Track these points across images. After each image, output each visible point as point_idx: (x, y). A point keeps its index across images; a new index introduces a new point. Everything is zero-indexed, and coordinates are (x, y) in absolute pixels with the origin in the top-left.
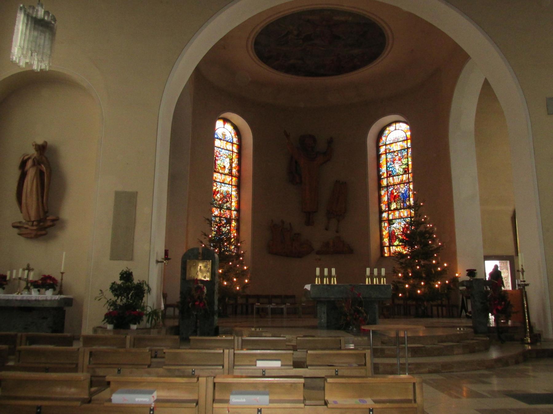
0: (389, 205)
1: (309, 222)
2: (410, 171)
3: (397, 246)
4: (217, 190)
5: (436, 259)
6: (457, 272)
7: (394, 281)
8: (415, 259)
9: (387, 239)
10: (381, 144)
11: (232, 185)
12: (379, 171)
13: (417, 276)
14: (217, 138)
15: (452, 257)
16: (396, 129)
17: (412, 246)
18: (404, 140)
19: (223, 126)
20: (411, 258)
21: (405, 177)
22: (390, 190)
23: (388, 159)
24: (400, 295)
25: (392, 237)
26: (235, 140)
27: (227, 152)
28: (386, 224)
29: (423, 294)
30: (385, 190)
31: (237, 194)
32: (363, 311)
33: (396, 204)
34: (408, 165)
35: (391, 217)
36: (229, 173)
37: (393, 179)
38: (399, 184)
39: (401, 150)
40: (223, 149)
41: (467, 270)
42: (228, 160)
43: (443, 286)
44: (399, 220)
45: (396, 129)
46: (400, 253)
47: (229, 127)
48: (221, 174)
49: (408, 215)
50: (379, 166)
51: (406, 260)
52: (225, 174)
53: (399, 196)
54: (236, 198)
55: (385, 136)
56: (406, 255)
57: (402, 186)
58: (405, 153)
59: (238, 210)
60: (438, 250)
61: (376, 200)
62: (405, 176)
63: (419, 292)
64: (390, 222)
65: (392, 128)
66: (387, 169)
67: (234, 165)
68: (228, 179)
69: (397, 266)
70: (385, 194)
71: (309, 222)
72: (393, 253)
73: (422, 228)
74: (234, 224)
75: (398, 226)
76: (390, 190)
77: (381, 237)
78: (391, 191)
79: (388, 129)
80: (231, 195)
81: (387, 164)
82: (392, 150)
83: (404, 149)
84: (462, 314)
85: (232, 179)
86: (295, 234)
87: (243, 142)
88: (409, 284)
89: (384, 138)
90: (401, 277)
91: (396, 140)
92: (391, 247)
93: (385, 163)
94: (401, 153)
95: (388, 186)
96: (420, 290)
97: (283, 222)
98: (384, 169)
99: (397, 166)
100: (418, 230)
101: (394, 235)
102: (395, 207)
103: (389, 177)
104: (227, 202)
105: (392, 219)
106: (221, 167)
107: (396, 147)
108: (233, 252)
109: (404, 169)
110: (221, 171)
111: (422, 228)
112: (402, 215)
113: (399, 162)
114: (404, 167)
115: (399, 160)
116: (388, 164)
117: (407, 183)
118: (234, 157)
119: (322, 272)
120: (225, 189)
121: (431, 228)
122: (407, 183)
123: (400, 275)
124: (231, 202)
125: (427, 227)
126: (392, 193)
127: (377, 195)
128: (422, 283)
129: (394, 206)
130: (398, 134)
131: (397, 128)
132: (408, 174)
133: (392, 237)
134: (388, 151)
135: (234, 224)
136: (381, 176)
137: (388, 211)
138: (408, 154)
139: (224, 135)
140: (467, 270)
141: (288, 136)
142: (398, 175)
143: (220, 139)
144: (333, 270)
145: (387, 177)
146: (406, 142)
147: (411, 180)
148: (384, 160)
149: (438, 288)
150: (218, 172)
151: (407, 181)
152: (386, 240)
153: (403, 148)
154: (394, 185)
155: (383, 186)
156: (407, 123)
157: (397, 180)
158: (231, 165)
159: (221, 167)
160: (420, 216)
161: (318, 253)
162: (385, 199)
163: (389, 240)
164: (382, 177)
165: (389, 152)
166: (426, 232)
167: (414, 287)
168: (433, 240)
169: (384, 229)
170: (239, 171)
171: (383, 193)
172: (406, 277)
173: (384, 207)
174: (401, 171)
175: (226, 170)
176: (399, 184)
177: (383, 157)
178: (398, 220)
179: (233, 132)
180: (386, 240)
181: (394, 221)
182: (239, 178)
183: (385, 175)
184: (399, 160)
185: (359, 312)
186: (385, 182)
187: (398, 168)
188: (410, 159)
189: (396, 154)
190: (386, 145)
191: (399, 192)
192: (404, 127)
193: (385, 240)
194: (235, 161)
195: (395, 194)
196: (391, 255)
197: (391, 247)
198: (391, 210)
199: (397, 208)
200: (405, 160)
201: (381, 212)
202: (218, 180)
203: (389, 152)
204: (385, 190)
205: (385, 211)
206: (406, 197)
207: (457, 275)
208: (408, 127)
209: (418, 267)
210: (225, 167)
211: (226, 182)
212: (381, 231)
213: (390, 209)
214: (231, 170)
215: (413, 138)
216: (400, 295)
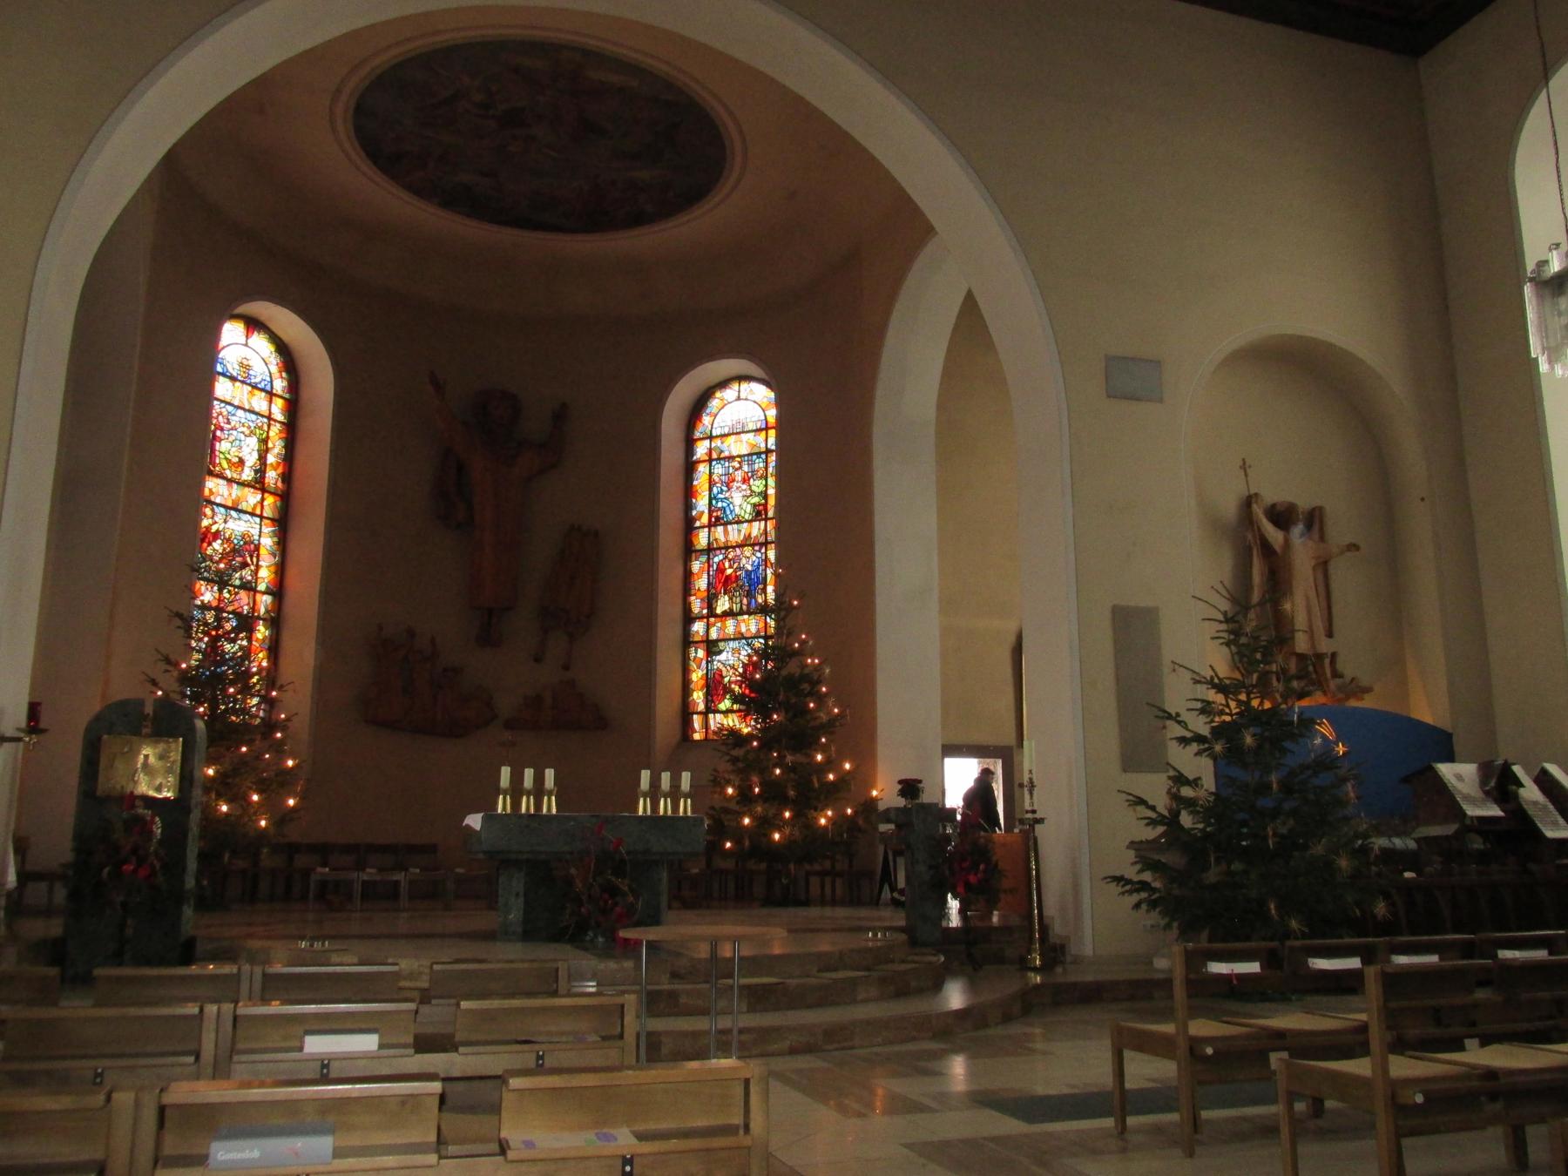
0: (710, 601)
1: (488, 634)
2: (771, 514)
3: (727, 712)
4: (214, 529)
5: (824, 749)
6: (873, 786)
7: (713, 808)
8: (771, 750)
9: (701, 694)
11: (261, 517)
12: (689, 507)
13: (775, 795)
16: (739, 398)
19: (243, 340)
21: (756, 529)
22: (716, 560)
23: (715, 477)
25: (715, 687)
26: (280, 385)
27: (254, 417)
28: (701, 653)
29: (788, 843)
30: (704, 559)
31: (278, 543)
34: (765, 496)
35: (714, 635)
36: (256, 480)
37: (726, 533)
38: (741, 546)
39: (751, 455)
40: (238, 407)
41: (900, 782)
42: (253, 443)
44: (734, 643)
45: (739, 398)
46: (733, 733)
48: (230, 481)
50: (689, 493)
57: (748, 551)
59: (278, 591)
60: (833, 720)
62: (756, 524)
63: (777, 836)
64: (712, 648)
65: (729, 394)
66: (710, 503)
67: (271, 459)
68: (251, 498)
69: (724, 766)
73: (792, 668)
74: (262, 632)
75: (732, 659)
76: (716, 560)
79: (718, 394)
80: (257, 548)
81: (710, 490)
82: (726, 454)
83: (759, 454)
85: (263, 499)
87: (305, 394)
89: (706, 420)
90: (732, 797)
94: (751, 463)
95: (710, 550)
96: (780, 831)
97: (411, 633)
98: (702, 503)
99: (737, 498)
100: (784, 673)
102: (727, 606)
104: (244, 565)
106: (229, 461)
108: (210, 544)
109: (755, 505)
110: (228, 474)
112: (743, 630)
114: (756, 500)
115: (745, 481)
117: (761, 545)
118: (272, 434)
119: (517, 778)
120: (238, 526)
121: (817, 668)
122: (761, 545)
123: (730, 791)
124: (258, 567)
126: (721, 570)
128: (787, 814)
129: (723, 604)
130: (743, 412)
131: (743, 395)
132: (766, 519)
133: (715, 687)
134: (715, 456)
135: (262, 632)
136: (693, 520)
137: (708, 617)
139: (246, 367)
140: (900, 782)
142: (739, 522)
143: (233, 379)
144: (550, 774)
145: (710, 525)
149: (825, 827)
150: (221, 476)
151: (762, 540)
152: (698, 697)
154: (727, 548)
157: (735, 534)
158: (262, 458)
159: (229, 461)
161: (509, 725)
162: (702, 583)
164: (698, 524)
165: (719, 459)
166: (805, 678)
168: (820, 699)
169: (693, 665)
170: (287, 477)
171: (696, 566)
172: (745, 797)
173: (697, 606)
174: (746, 511)
176: (741, 546)
177: (703, 469)
179: (274, 361)
180: (698, 697)
181: (721, 644)
182: (285, 497)
183: (705, 519)
184: (745, 481)
185: (613, 891)
186: (702, 539)
187: (740, 502)
188: (771, 482)
190: (711, 438)
193: (695, 695)
194: (277, 447)
195: (729, 571)
196: (711, 736)
198: (716, 616)
199: (731, 609)
200: (758, 483)
201: (689, 619)
202: (218, 500)
204: (704, 559)
205: (701, 618)
206: (754, 583)
207: (874, 793)
210: (241, 462)
211: (243, 506)
212: (686, 671)
213: (712, 613)
214: (261, 471)
215: (782, 425)
216: (728, 845)
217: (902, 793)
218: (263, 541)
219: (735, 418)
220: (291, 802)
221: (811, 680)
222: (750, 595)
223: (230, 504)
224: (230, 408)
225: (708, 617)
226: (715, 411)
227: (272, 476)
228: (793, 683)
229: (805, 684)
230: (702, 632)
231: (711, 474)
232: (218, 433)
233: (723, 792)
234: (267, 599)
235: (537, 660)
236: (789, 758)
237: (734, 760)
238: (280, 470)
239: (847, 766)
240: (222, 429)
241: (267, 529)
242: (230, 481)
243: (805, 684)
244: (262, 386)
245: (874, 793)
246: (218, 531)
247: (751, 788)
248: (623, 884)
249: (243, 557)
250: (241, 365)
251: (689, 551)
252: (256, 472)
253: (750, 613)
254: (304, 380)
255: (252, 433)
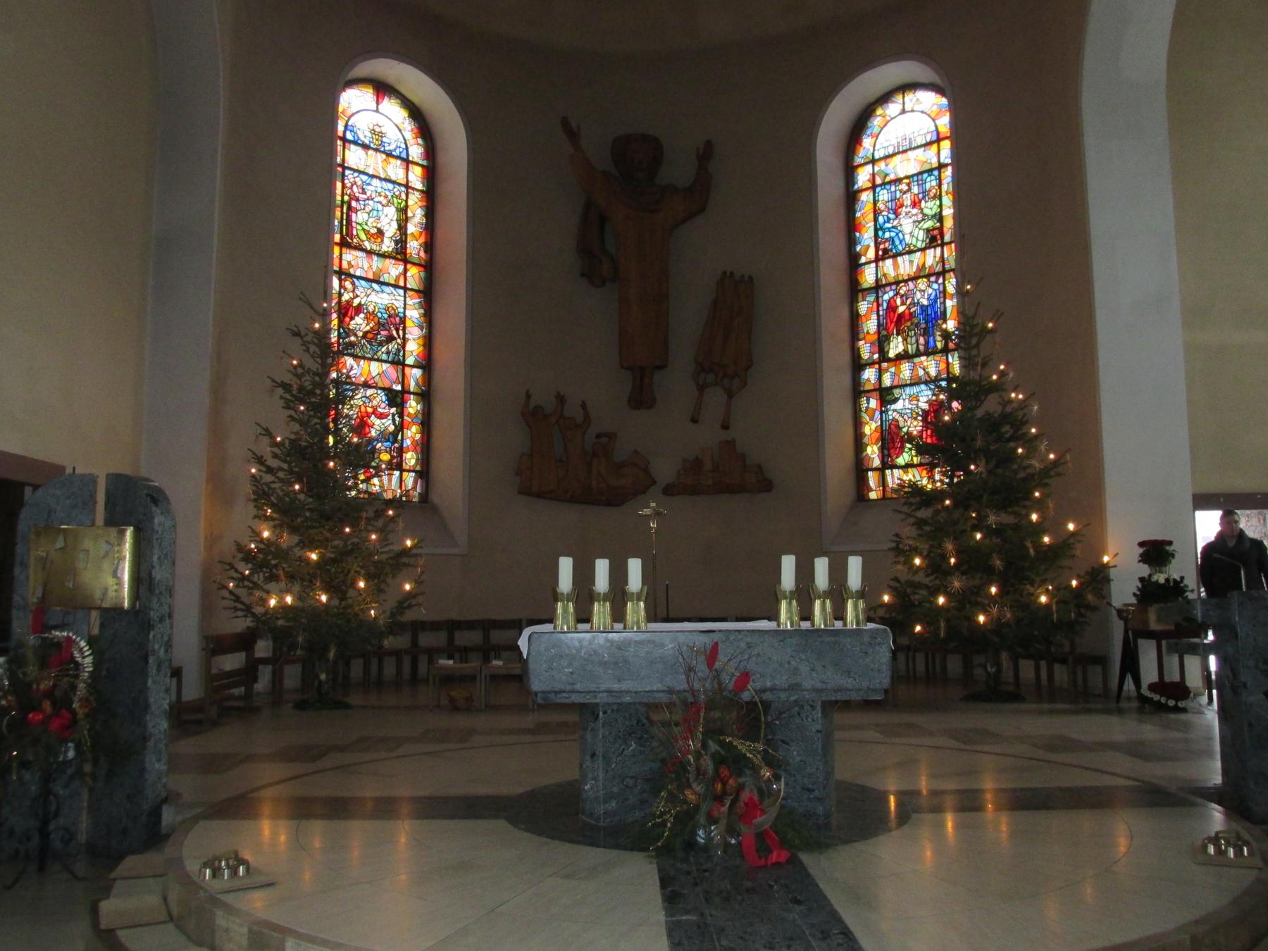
0: (881, 343)
1: (641, 398)
2: (947, 238)
3: (908, 466)
4: (356, 302)
5: (1039, 506)
6: (1103, 551)
7: (896, 579)
8: (967, 508)
9: (875, 448)
10: (858, 160)
11: (405, 289)
12: (852, 241)
13: (974, 562)
14: (355, 143)
15: (1090, 502)
16: (903, 112)
17: (955, 463)
18: (930, 144)
20: (956, 504)
21: (931, 257)
22: (886, 297)
23: (881, 206)
24: (918, 628)
25: (891, 439)
26: (416, 152)
27: (390, 186)
28: (873, 403)
29: (997, 627)
30: (872, 298)
31: (424, 315)
32: (758, 760)
33: (905, 339)
34: (940, 218)
35: (887, 381)
36: (397, 251)
37: (896, 266)
38: (914, 278)
39: (921, 173)
40: (373, 176)
41: (1141, 544)
42: (391, 212)
43: (1064, 597)
44: (913, 392)
45: (903, 112)
46: (916, 489)
47: (393, 110)
48: (370, 253)
49: (939, 373)
50: (852, 227)
51: (937, 512)
52: (383, 256)
53: (911, 315)
54: (421, 328)
55: (872, 135)
56: (937, 496)
57: (922, 283)
58: (931, 183)
59: (426, 363)
60: (1050, 470)
61: (844, 333)
62: (930, 252)
63: (982, 619)
64: (886, 396)
65: (893, 108)
66: (876, 235)
67: (412, 228)
68: (393, 270)
69: (908, 531)
70: (870, 311)
71: (641, 398)
72: (894, 490)
73: (991, 405)
74: (413, 406)
75: (909, 408)
76: (886, 297)
77: (859, 445)
78: (889, 302)
79: (879, 111)
80: (403, 320)
81: (876, 220)
82: (892, 177)
83: (930, 171)
84: (1125, 687)
85: (406, 271)
86: (599, 436)
87: (442, 158)
88: (947, 595)
89: (867, 142)
90: (919, 568)
91: (906, 145)
92: (888, 472)
93: (871, 216)
94: (921, 184)
95: (878, 287)
96: (985, 612)
97: (561, 399)
98: (866, 237)
99: (906, 225)
100: (980, 413)
101: (898, 434)
102: (901, 348)
103: (883, 259)
104: (390, 339)
105: (892, 388)
106: (367, 233)
107: (903, 167)
108: (352, 318)
109: (928, 231)
110: (367, 245)
111: (991, 405)
112: (921, 372)
113: (915, 211)
114: (929, 224)
115: (915, 204)
116: (881, 219)
117: (938, 275)
118: (410, 202)
119: (584, 576)
120: (380, 299)
121: (1023, 405)
122: (938, 275)
123: (917, 561)
124: (405, 340)
125: (1010, 401)
126: (892, 307)
127: (845, 313)
128: (993, 590)
129: (896, 346)
130: (911, 129)
131: (908, 108)
132: (942, 245)
133: (891, 439)
134: (878, 181)
135: (413, 406)
136: (858, 256)
137: (879, 362)
138: (940, 185)
139: (378, 134)
140: (1141, 544)
141: (572, 134)
142: (910, 252)
143: (366, 147)
144: (635, 567)
145: (877, 260)
146: (935, 147)
147: (951, 263)
148: (870, 207)
149: (1048, 606)
150: (359, 248)
151: (939, 268)
152: (873, 451)
153: (927, 167)
154: (897, 283)
155: (865, 286)
156: (939, 90)
157: (906, 266)
158: (402, 227)
159: (367, 233)
160: (984, 365)
161: (669, 491)
162: (871, 326)
163: (882, 449)
164: (863, 260)
165: (884, 184)
166: (1006, 418)
167: (968, 601)
168: (1030, 442)
169: (866, 417)
170: (429, 246)
171: (863, 307)
172: (936, 566)
173: (866, 351)
174: (919, 238)
175: (387, 241)
176: (914, 278)
177: (866, 197)
178: (908, 390)
179: (408, 127)
180: (873, 451)
181: (897, 392)
182: (428, 267)
183: (871, 254)
184: (915, 204)
185: (737, 763)
186: (868, 276)
187: (910, 229)
188: (947, 201)
189: (904, 187)
190: (873, 161)
191: (913, 304)
192: (929, 100)
193: (869, 450)
194: (417, 215)
195: (901, 309)
196: (889, 495)
197: (888, 472)
198: (889, 360)
199: (906, 351)
200: (930, 204)
201: (858, 365)
202: (358, 273)
203: (884, 184)
204: (872, 298)
205: (871, 364)
206: (933, 316)
207: (1106, 559)
208: (944, 101)
209: (979, 536)
210: (380, 233)
211: (385, 278)
212: (858, 424)
213: (884, 357)
214: (401, 242)
215: (959, 134)
216: (918, 628)
217: (1145, 558)
218: (408, 313)
219: (900, 134)
220: (408, 587)
221: (1014, 421)
222: (926, 333)
223: (371, 276)
224: (364, 178)
225: (879, 362)
226: (876, 130)
227: (414, 247)
228: (992, 425)
229: (1009, 425)
230: (873, 379)
231: (875, 202)
232: (354, 204)
233: (908, 562)
234: (417, 373)
235: (694, 421)
236: (992, 519)
237: (920, 523)
238: (422, 240)
239: (1071, 527)
240: (357, 200)
241: (413, 301)
242: (370, 253)
243: (1009, 425)
244: (396, 153)
245: (1106, 559)
246: (360, 305)
247: (945, 558)
248: (749, 749)
249: (389, 330)
250: (373, 132)
251: (855, 290)
252: (397, 242)
253: (927, 354)
254: (440, 143)
255: (389, 203)
